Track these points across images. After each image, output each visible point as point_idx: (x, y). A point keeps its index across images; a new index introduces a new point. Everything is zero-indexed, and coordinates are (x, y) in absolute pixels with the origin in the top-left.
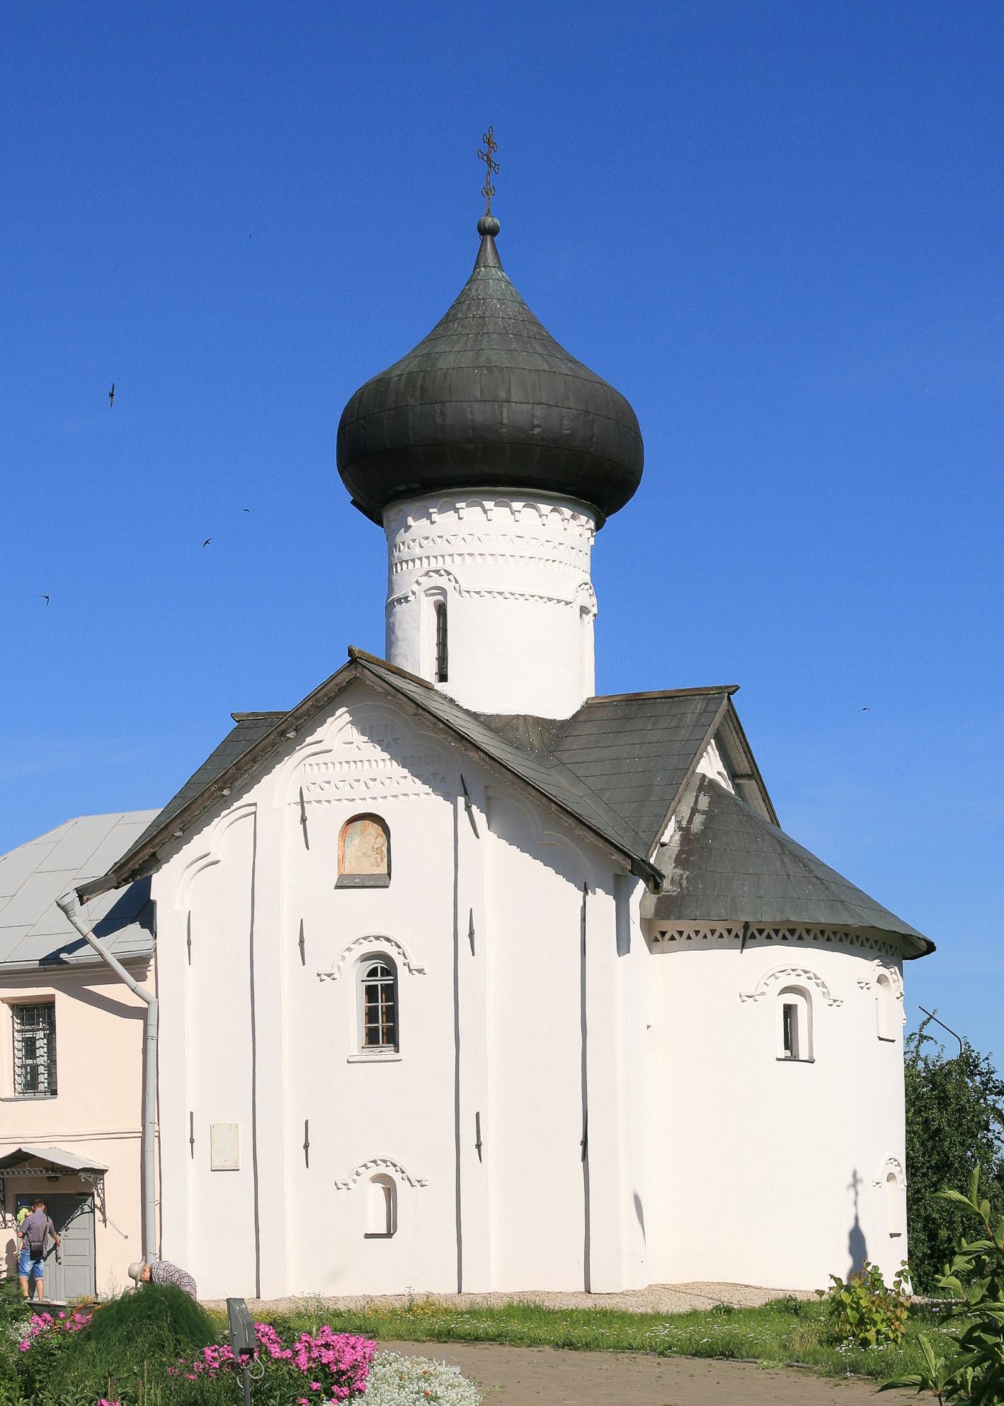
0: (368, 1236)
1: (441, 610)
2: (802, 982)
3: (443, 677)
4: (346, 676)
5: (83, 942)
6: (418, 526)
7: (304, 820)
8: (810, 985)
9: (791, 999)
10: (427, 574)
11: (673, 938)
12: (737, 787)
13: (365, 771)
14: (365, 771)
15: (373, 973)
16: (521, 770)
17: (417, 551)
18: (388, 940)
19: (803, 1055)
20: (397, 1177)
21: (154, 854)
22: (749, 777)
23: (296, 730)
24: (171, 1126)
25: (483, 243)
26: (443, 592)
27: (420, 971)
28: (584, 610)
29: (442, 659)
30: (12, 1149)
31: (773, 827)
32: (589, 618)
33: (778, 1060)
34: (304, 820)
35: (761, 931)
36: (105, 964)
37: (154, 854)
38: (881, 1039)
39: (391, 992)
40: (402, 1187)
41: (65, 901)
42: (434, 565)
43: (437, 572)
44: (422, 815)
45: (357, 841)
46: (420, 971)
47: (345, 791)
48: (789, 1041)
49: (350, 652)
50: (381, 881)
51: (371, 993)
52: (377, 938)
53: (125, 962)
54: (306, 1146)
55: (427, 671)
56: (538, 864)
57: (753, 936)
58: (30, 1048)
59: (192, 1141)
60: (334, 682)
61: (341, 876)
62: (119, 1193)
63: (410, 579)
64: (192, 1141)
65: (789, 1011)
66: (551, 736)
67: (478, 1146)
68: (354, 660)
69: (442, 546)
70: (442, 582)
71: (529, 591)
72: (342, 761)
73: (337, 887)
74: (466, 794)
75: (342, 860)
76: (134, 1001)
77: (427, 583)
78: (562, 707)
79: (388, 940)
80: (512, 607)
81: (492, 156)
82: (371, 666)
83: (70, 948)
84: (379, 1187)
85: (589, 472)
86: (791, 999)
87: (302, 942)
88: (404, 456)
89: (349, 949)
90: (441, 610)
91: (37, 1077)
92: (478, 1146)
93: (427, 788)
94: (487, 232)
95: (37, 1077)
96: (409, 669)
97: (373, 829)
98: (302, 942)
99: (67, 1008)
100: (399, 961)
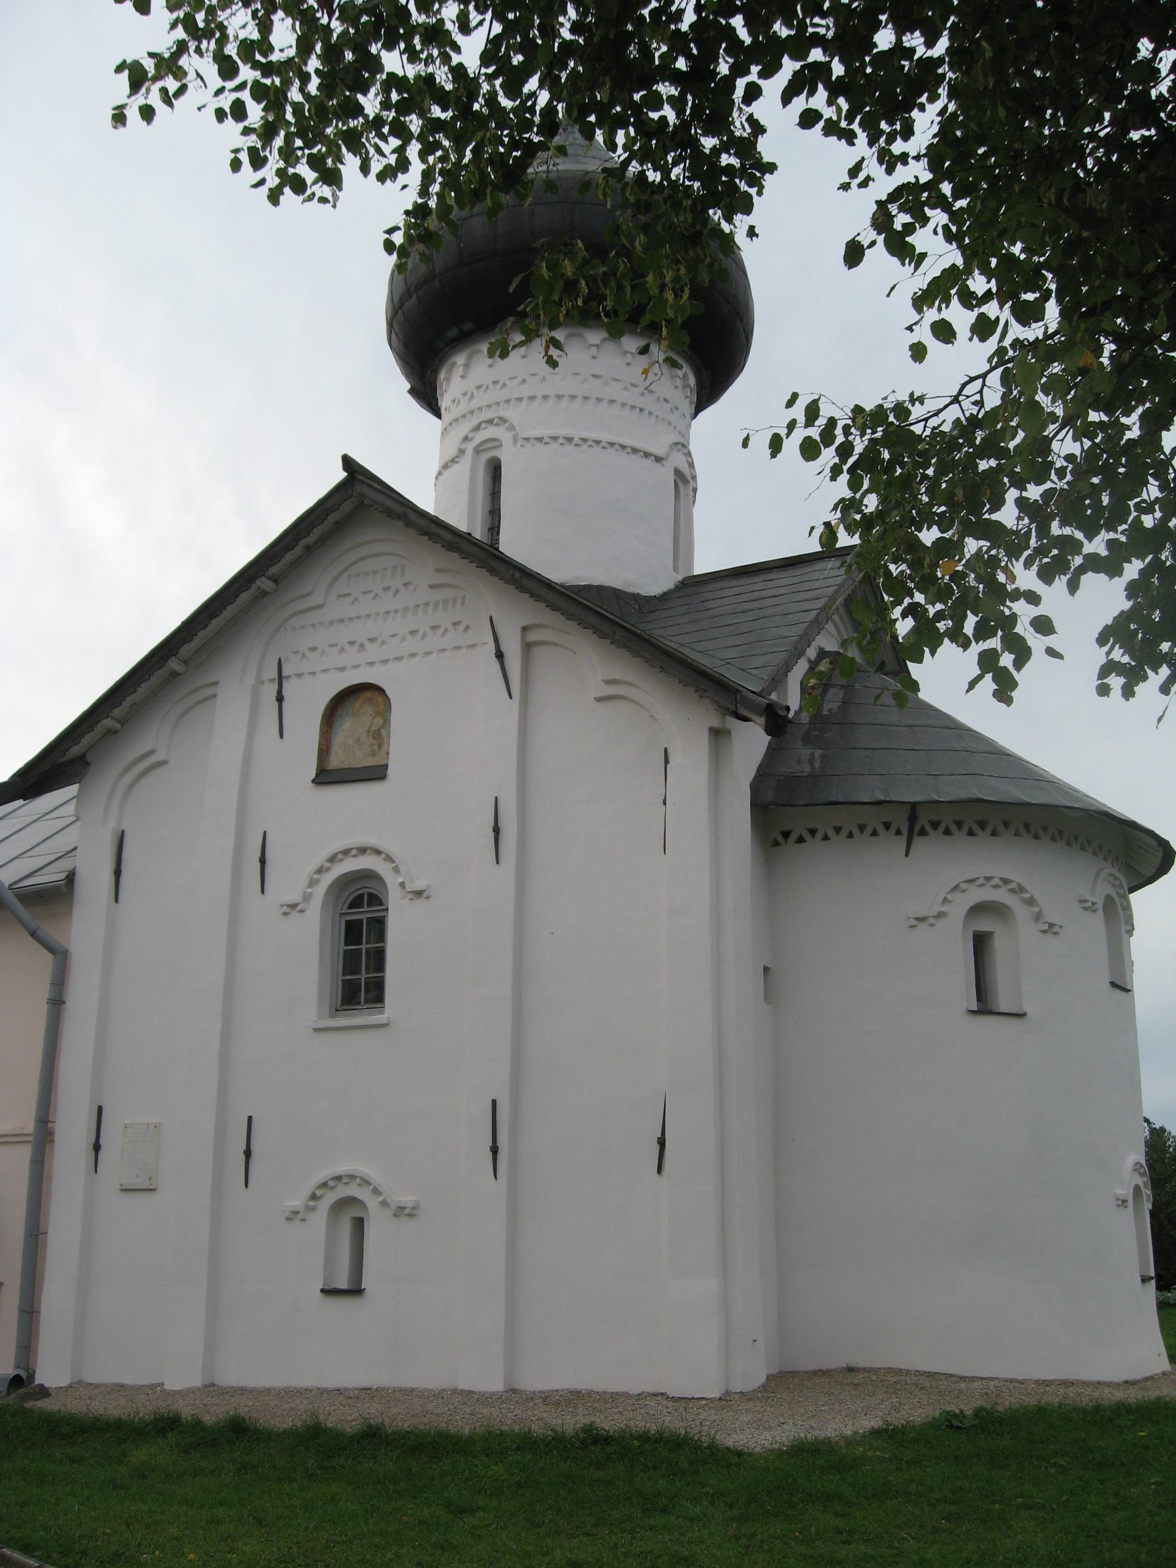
2: (1000, 895)
18: (378, 852)
19: (1004, 1003)
29: (494, 513)
39: (379, 926)
49: (348, 463)
52: (363, 851)
57: (923, 832)
65: (981, 943)
75: (324, 752)
86: (983, 925)
100: (392, 882)
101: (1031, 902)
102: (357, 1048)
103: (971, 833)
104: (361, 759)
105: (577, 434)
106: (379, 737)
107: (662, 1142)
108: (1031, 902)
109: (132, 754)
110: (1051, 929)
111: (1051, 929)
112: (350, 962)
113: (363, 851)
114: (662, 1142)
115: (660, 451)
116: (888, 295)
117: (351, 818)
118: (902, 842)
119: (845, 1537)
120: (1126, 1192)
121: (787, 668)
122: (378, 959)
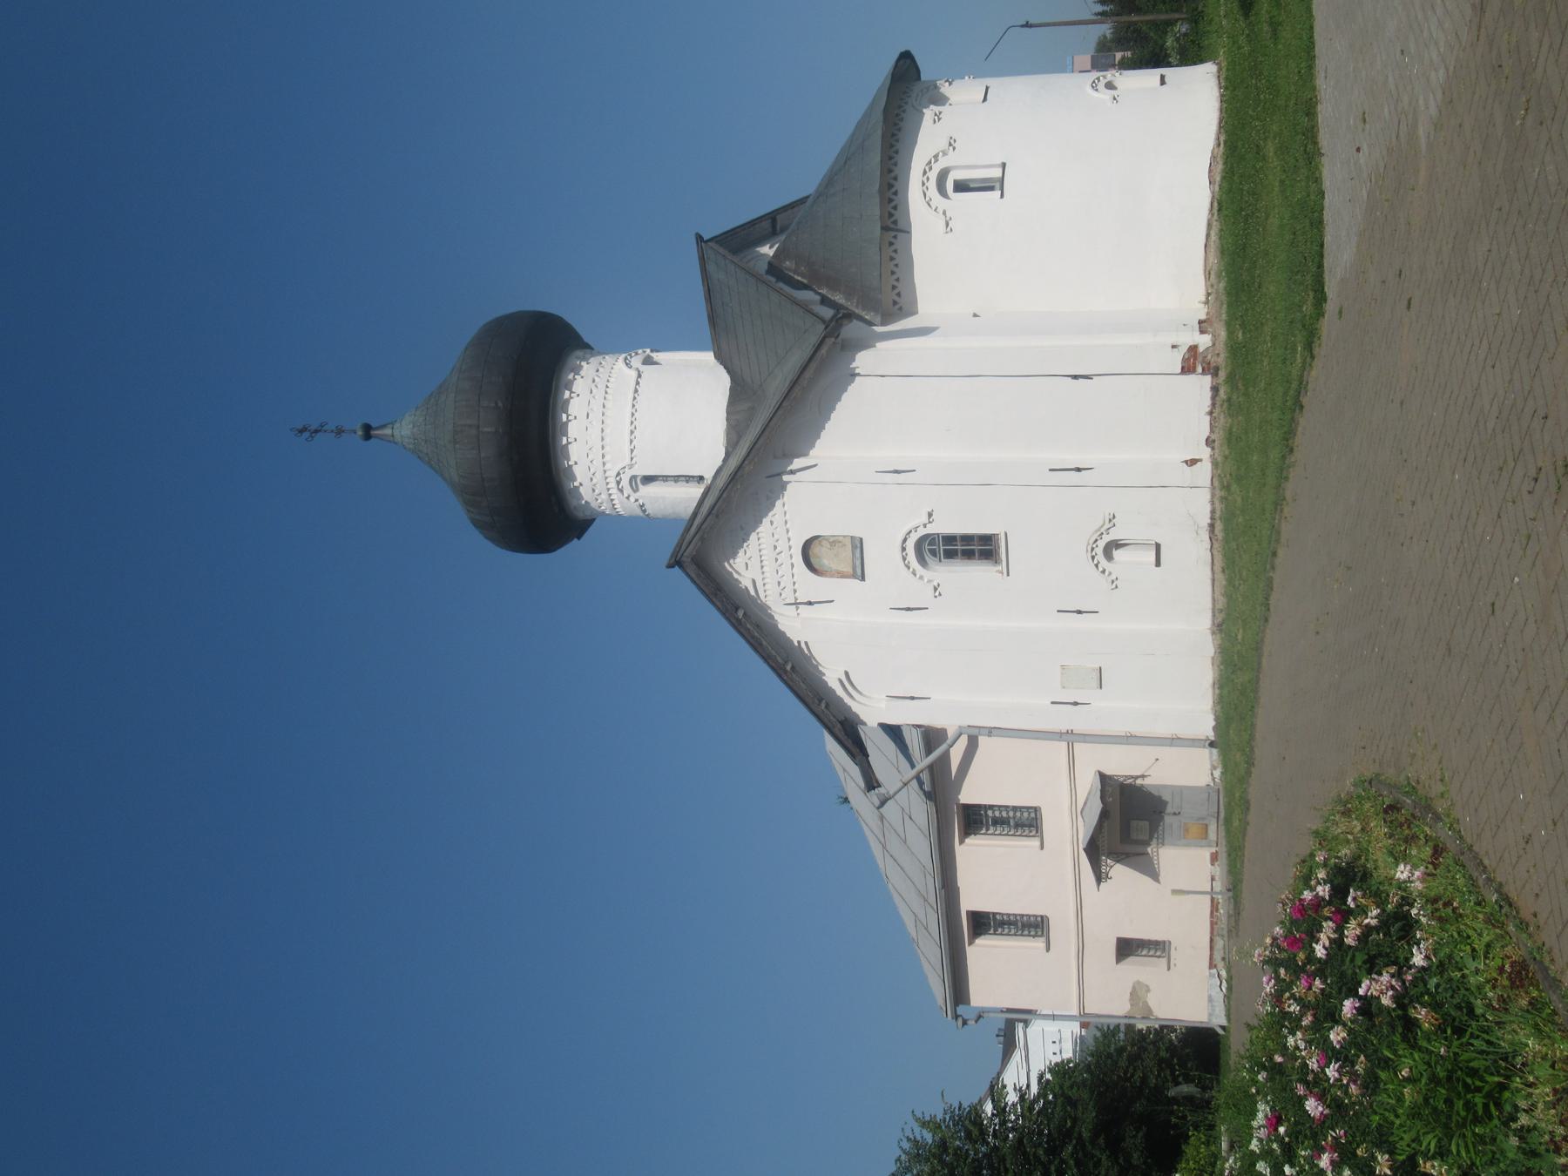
0: (1158, 564)
1: (648, 479)
2: (933, 175)
3: (701, 478)
4: (692, 569)
5: (918, 778)
6: (586, 494)
7: (810, 603)
8: (937, 168)
9: (950, 186)
10: (621, 491)
11: (899, 295)
12: (782, 231)
13: (768, 553)
14: (768, 553)
15: (933, 553)
16: (771, 410)
17: (604, 496)
18: (905, 540)
19: (997, 173)
20: (1106, 539)
21: (841, 723)
22: (774, 221)
23: (737, 609)
24: (1064, 720)
25: (377, 437)
26: (633, 478)
27: (930, 515)
28: (648, 361)
29: (688, 479)
30: (1083, 856)
31: (810, 201)
32: (656, 356)
33: (1048, 949)
34: (810, 603)
35: (891, 215)
36: (931, 767)
37: (841, 723)
38: (985, 99)
39: (949, 539)
40: (1114, 535)
41: (877, 803)
42: (613, 485)
43: (618, 483)
44: (810, 499)
45: (826, 562)
46: (930, 515)
47: (785, 569)
48: (986, 186)
49: (670, 566)
50: (858, 545)
51: (950, 555)
52: (904, 549)
53: (929, 751)
54: (1079, 612)
55: (696, 491)
56: (845, 397)
57: (895, 222)
58: (997, 822)
59: (1076, 704)
60: (772, 401)
61: (854, 576)
62: (1123, 763)
63: (623, 503)
64: (1076, 704)
65: (961, 187)
66: (740, 394)
67: (1079, 470)
68: (676, 562)
69: (598, 478)
70: (625, 483)
71: (629, 409)
72: (763, 563)
73: (863, 579)
74: (780, 475)
75: (843, 575)
76: (962, 743)
77: (627, 490)
78: (721, 382)
79: (905, 540)
80: (642, 425)
81: (313, 428)
82: (689, 537)
83: (921, 784)
84: (1116, 553)
85: (529, 365)
86: (950, 186)
87: (908, 609)
88: (531, 502)
89: (914, 574)
90: (648, 479)
91: (1025, 822)
92: (1079, 470)
93: (778, 503)
94: (368, 431)
95: (1025, 822)
96: (691, 510)
97: (815, 550)
98: (908, 609)
99: (970, 794)
100: (922, 532)
101: (936, 157)
102: (1017, 550)
103: (896, 193)
104: (847, 552)
105: (628, 428)
106: (834, 542)
107: (1075, 377)
108: (936, 157)
109: (840, 692)
110: (951, 144)
111: (951, 144)
112: (968, 555)
113: (904, 549)
114: (1075, 377)
115: (634, 374)
116: (1158, 564)
117: (884, 556)
118: (900, 235)
119: (975, 1132)
120: (1105, 95)
121: (795, 302)
122: (967, 539)
